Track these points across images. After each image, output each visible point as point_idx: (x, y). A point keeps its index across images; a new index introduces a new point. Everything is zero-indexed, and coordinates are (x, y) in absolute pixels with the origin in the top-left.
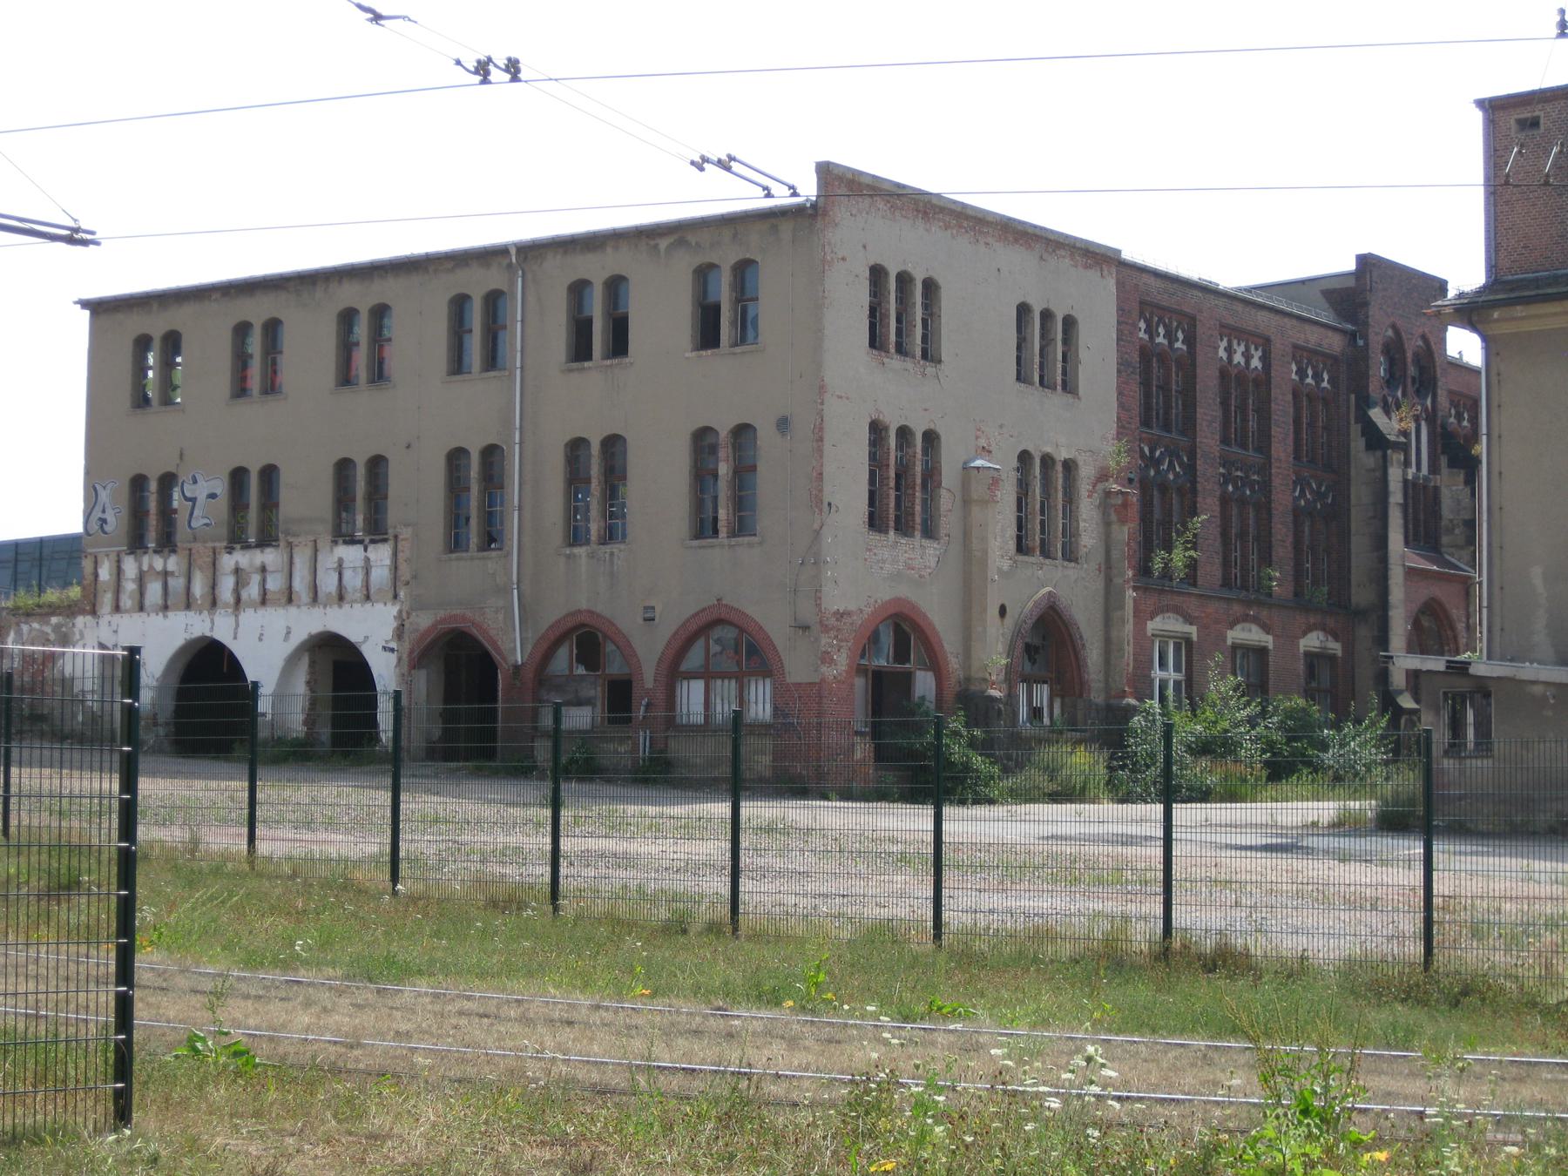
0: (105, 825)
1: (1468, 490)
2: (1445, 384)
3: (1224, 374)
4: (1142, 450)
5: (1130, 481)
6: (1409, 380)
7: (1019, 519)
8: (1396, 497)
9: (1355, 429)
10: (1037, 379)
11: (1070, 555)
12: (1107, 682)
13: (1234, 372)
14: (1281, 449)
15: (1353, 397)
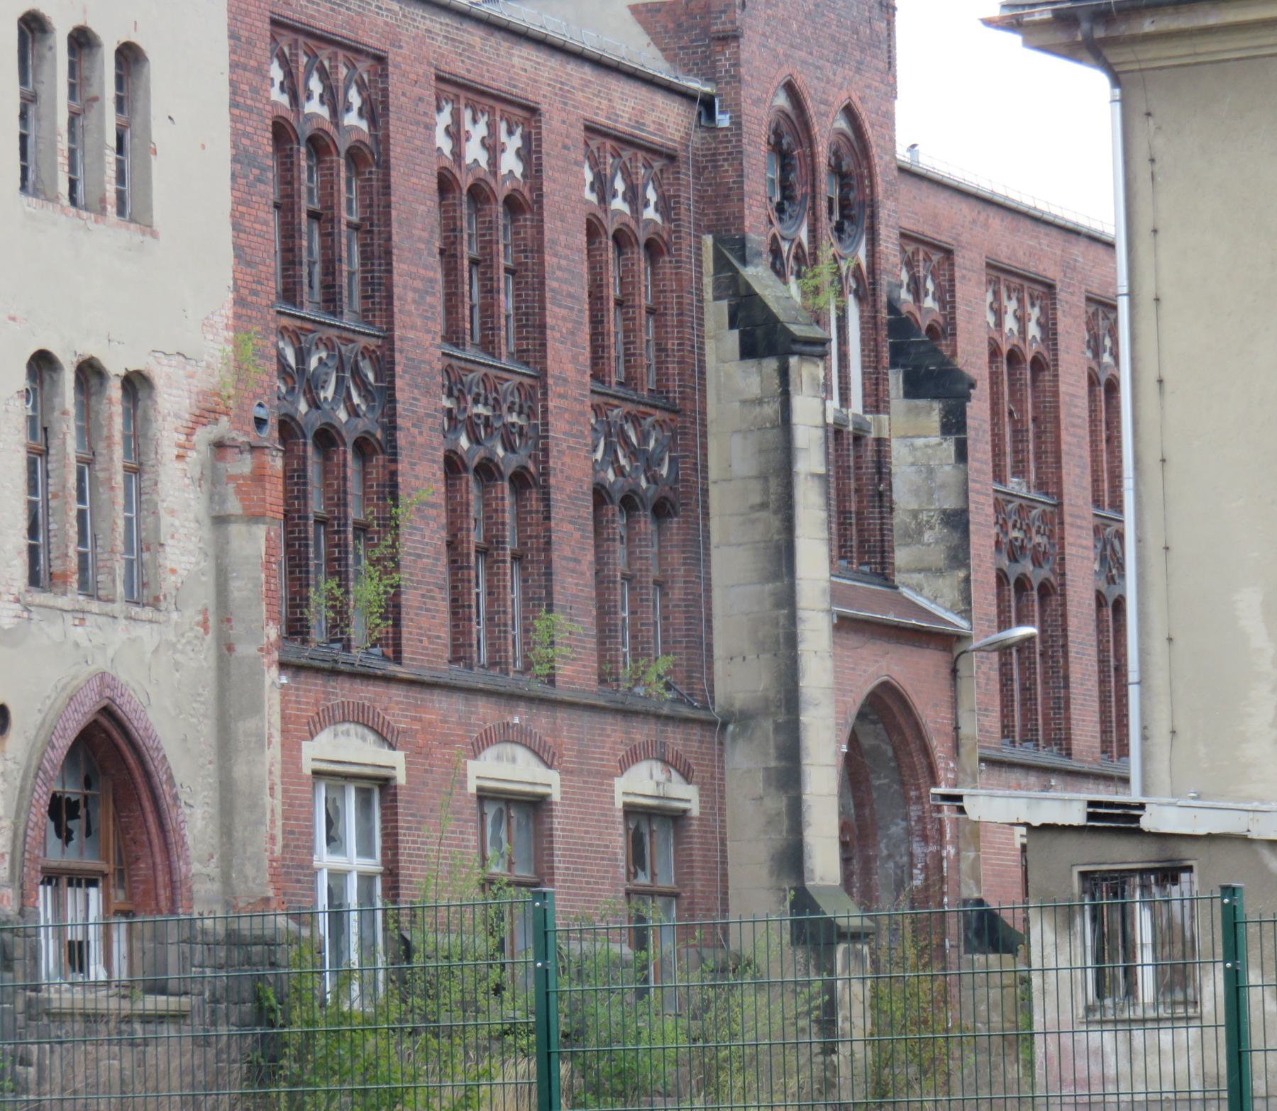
0: (1051, 1014)
1: (949, 446)
2: (897, 211)
3: (446, 183)
4: (281, 357)
5: (260, 423)
6: (823, 205)
7: (32, 506)
8: (811, 459)
9: (716, 312)
10: (64, 187)
11: (142, 591)
12: (226, 879)
13: (466, 181)
14: (567, 355)
15: (708, 240)
